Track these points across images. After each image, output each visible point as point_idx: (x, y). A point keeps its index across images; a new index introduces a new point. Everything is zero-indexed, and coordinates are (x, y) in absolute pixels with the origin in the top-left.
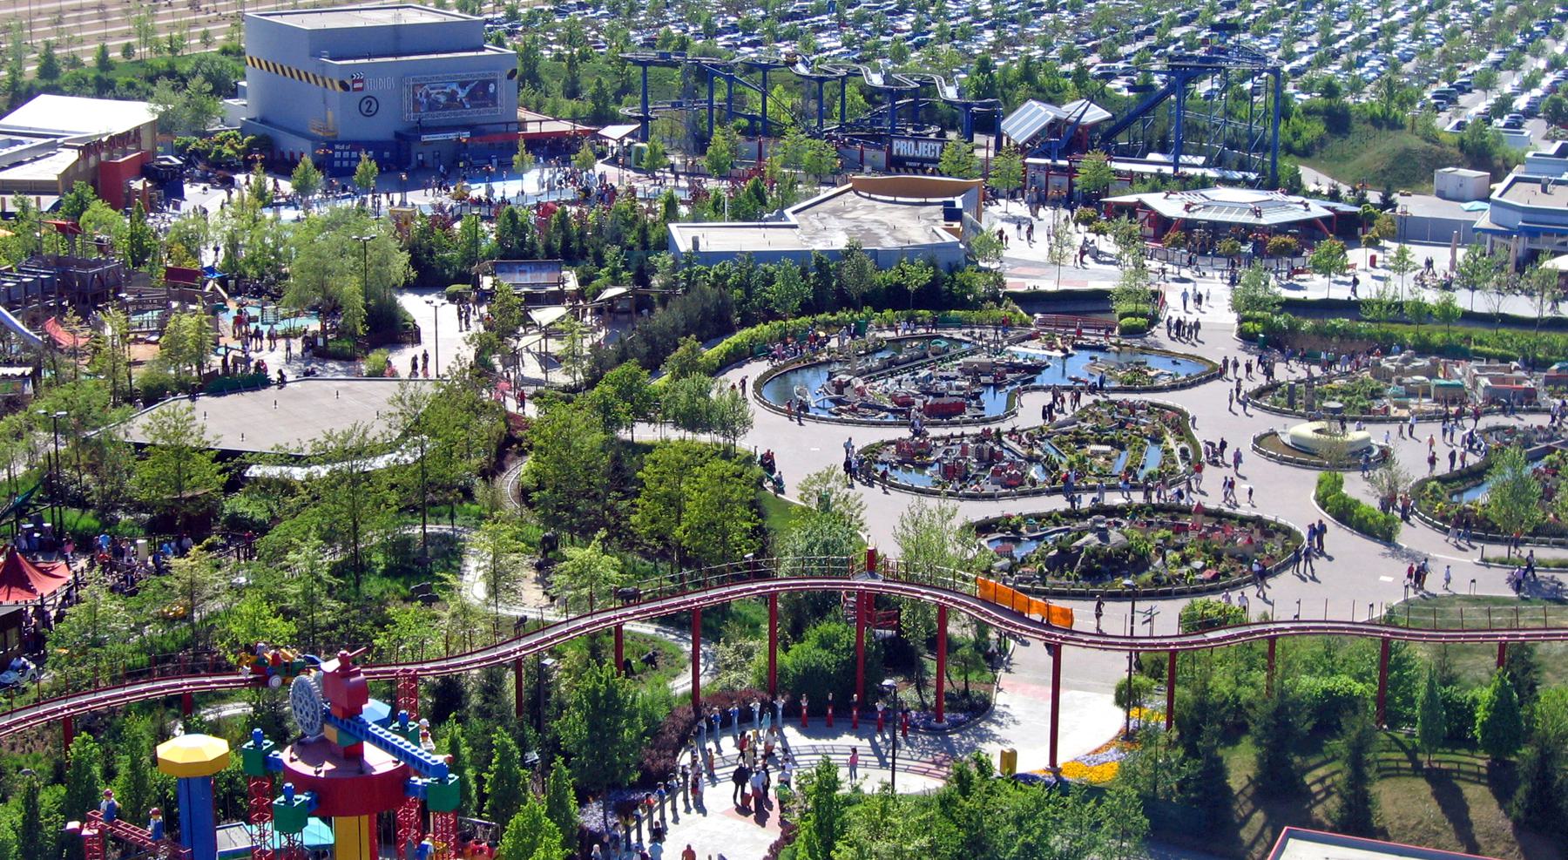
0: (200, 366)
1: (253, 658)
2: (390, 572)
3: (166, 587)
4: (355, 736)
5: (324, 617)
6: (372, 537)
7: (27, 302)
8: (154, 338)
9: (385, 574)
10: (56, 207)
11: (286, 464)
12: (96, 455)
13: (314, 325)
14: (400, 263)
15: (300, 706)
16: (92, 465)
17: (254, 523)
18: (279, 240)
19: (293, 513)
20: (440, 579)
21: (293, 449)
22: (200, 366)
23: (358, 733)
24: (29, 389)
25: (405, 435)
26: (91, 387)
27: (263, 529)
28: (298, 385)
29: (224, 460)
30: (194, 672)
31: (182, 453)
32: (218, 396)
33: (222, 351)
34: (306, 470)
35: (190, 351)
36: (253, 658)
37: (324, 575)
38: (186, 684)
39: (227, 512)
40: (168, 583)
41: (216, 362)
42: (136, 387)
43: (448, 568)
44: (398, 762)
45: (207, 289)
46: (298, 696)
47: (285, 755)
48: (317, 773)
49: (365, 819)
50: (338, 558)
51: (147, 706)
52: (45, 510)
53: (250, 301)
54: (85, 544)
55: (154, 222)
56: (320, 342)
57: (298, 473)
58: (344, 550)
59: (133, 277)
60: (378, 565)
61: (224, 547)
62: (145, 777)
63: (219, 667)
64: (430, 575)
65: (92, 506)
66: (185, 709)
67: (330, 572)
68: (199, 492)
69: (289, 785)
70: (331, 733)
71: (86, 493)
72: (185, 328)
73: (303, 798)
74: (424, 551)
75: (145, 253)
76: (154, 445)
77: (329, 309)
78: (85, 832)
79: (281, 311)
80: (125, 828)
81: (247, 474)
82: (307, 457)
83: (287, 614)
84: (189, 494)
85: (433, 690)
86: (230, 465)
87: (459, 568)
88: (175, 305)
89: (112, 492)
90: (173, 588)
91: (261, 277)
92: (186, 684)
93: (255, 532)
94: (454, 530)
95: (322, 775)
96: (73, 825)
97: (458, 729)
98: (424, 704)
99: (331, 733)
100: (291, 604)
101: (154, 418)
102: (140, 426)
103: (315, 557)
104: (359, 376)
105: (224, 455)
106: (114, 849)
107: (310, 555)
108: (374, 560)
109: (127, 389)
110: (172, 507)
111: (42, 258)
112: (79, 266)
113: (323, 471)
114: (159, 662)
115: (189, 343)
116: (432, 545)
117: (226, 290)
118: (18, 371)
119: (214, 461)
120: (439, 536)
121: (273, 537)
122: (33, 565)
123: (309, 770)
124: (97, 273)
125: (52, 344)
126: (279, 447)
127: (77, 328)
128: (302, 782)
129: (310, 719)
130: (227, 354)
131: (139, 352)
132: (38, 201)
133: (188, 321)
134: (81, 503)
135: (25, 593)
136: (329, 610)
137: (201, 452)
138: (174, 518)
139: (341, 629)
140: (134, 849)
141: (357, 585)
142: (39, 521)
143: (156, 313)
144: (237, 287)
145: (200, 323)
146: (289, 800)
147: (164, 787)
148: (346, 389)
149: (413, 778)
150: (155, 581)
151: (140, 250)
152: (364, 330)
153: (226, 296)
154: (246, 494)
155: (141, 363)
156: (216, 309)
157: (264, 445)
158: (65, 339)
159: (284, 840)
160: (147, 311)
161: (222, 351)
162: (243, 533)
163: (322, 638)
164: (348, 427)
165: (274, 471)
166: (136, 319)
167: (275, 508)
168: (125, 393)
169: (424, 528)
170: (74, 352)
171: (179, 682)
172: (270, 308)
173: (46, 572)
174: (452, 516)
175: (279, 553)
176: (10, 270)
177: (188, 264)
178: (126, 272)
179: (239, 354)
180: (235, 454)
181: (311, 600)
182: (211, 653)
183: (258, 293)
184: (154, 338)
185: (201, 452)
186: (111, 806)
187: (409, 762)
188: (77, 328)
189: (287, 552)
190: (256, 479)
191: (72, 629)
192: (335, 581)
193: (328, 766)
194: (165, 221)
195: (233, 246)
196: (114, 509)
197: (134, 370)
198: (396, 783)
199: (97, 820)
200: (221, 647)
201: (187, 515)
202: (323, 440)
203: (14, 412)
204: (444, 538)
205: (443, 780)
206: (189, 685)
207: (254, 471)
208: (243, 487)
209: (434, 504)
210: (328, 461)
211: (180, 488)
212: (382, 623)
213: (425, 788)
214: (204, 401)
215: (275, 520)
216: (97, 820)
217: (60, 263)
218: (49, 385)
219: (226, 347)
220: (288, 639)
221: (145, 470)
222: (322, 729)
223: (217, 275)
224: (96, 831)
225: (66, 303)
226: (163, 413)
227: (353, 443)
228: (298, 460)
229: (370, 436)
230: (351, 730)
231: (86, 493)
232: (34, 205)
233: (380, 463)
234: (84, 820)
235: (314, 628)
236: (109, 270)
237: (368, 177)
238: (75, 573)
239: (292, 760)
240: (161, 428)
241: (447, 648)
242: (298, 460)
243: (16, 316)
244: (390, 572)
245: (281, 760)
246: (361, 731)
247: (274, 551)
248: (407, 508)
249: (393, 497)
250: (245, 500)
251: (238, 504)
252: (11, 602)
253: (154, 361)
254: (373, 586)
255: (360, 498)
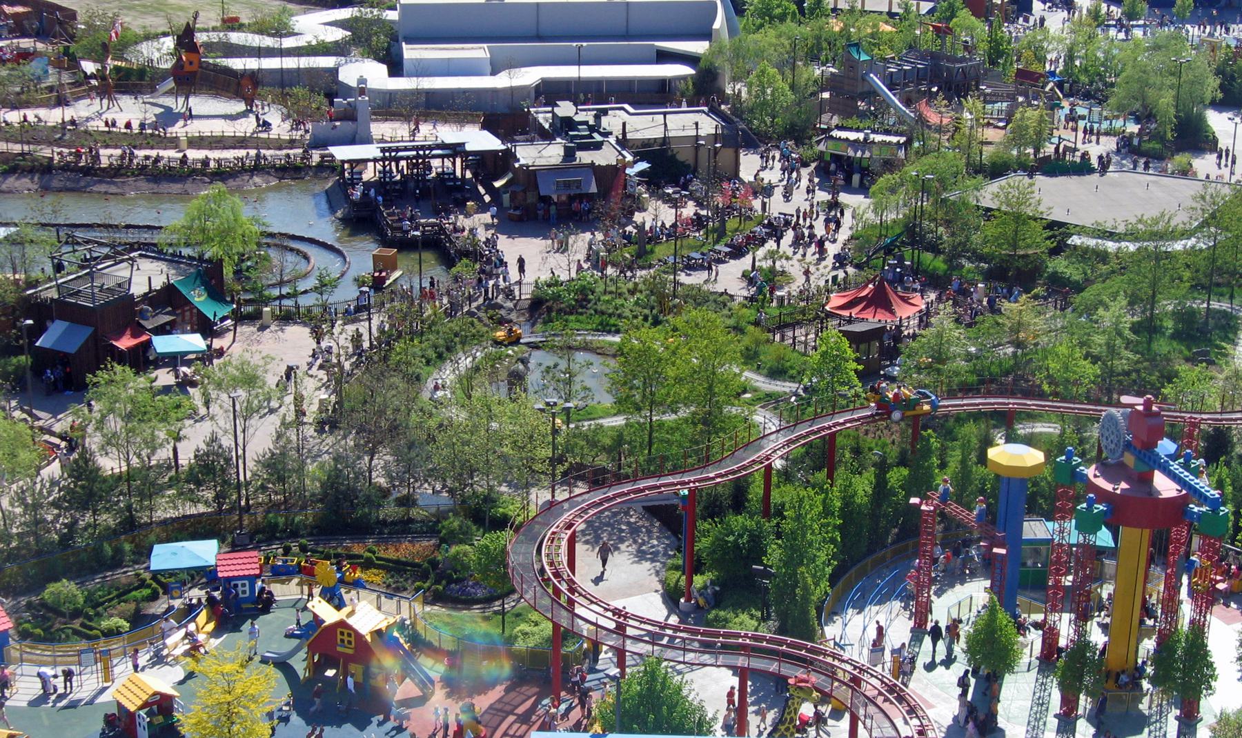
0: (1037, 150)
1: (878, 397)
2: (1176, 336)
3: (998, 324)
4: (1148, 465)
5: (1121, 365)
6: (1168, 305)
7: (906, 85)
8: (1001, 124)
9: (1174, 337)
10: (931, 12)
11: (1099, 238)
12: (953, 215)
13: (1132, 128)
14: (1212, 84)
15: (1107, 434)
16: (947, 221)
17: (1070, 282)
18: (1109, 57)
19: (1106, 277)
20: (1218, 347)
21: (1109, 226)
22: (1037, 150)
23: (1151, 463)
24: (901, 154)
25: (1201, 226)
26: (951, 158)
27: (1079, 288)
28: (1116, 175)
29: (1052, 229)
30: (1013, 394)
31: (1020, 219)
32: (1079, 175)
33: (1055, 140)
34: (1117, 245)
35: (1031, 137)
36: (878, 397)
37: (1127, 332)
38: (1012, 403)
39: (1050, 270)
40: (1000, 321)
41: (1049, 149)
42: (984, 162)
43: (1226, 338)
44: (1181, 491)
45: (1047, 89)
46: (1106, 426)
47: (1090, 471)
48: (1114, 489)
49: (1147, 532)
50: (1136, 319)
51: (977, 416)
52: (907, 252)
53: (1081, 102)
54: (934, 281)
55: (1008, 30)
56: (1136, 142)
57: (1111, 246)
58: (1143, 312)
59: (989, 74)
60: (1167, 329)
61: (1045, 298)
62: (971, 471)
63: (1034, 392)
64: (1210, 342)
65: (943, 253)
66: (1006, 420)
67: (1130, 329)
68: (1030, 252)
69: (1091, 495)
70: (1129, 459)
71: (939, 242)
72: (1029, 119)
73: (1101, 508)
74: (1206, 323)
75: (1000, 54)
76: (999, 210)
77: (1145, 116)
78: (924, 507)
79: (1105, 113)
80: (953, 508)
81: (1069, 242)
82: (1119, 234)
83: (1095, 359)
84: (1022, 253)
85: (1208, 438)
86: (1056, 233)
87: (1233, 341)
88: (1021, 99)
89: (959, 244)
90: (1003, 325)
91: (1091, 83)
92: (1012, 403)
93: (1071, 289)
94: (1232, 308)
95: (1118, 492)
96: (914, 500)
97: (1225, 470)
98: (1197, 445)
99: (1129, 459)
100: (1095, 351)
101: (1001, 188)
102: (990, 194)
103: (1120, 316)
104: (1163, 172)
105: (1053, 225)
106: (939, 523)
107: (1117, 314)
108: (1165, 324)
109: (977, 163)
110: (1008, 261)
111: (919, 51)
112: (948, 61)
113: (1132, 247)
114: (984, 382)
115: (1031, 131)
116: (1213, 318)
117: (1062, 92)
118: (894, 139)
119: (1044, 228)
120: (1219, 312)
121: (1088, 294)
122: (896, 293)
123: (1108, 487)
124: (962, 67)
125: (922, 121)
126: (1098, 224)
127: (943, 110)
128: (1102, 495)
129: (1113, 446)
130: (1060, 143)
131: (990, 134)
132: (918, 5)
133: (1031, 115)
134: (935, 249)
135: (888, 314)
136: (1126, 359)
137: (1035, 219)
138: (1007, 270)
139: (1134, 376)
140: (954, 525)
141: (1150, 342)
142: (901, 260)
143: (1005, 104)
144: (1071, 89)
145: (1042, 116)
146: (1090, 507)
147: (983, 481)
148: (1154, 182)
149: (1191, 506)
150: (989, 318)
151: (996, 52)
152: (1172, 136)
153: (1061, 96)
154: (1067, 258)
155: (990, 143)
156: (1053, 106)
157: (1088, 222)
158: (933, 118)
159: (1081, 538)
160: (997, 102)
161: (1055, 140)
162: (1061, 289)
163: (1118, 381)
164: (1155, 213)
165: (1092, 242)
166: (989, 107)
167: (1089, 272)
168: (976, 166)
169: (1208, 304)
170: (940, 129)
171: (1006, 401)
172: (1096, 109)
173: (905, 300)
174: (1232, 297)
175: (1090, 310)
176: (893, 58)
177: (1035, 67)
178: (984, 69)
179: (1070, 145)
180: (1061, 225)
181: (1111, 348)
182: (1027, 381)
183: (1087, 96)
184: (1001, 124)
185: (1035, 219)
186: (946, 490)
187: (1191, 492)
188: (943, 110)
189: (1097, 309)
190: (1075, 247)
191: (922, 347)
192: (1132, 337)
193: (1124, 485)
194: (1015, 31)
195: (1070, 58)
196: (960, 256)
197: (985, 148)
198: (1177, 508)
199: (933, 499)
200: (1039, 377)
201: (1018, 269)
202: (1133, 220)
203: (892, 172)
204: (1224, 314)
205: (1215, 510)
206: (1014, 404)
207: (1075, 240)
208: (1064, 251)
209: (1218, 285)
210: (1136, 239)
211: (1015, 246)
212: (1170, 377)
213: (1201, 515)
214: (1040, 179)
215: (1088, 282)
216: (933, 499)
217: (934, 57)
218: (917, 153)
219: (1060, 138)
220: (1092, 378)
221: (991, 229)
222: (1122, 455)
223: (1057, 79)
224: (932, 508)
225: (935, 89)
226: (1009, 185)
227: (1161, 226)
228: (1111, 236)
229: (1173, 223)
230: (1146, 460)
231: (939, 242)
232: (914, 8)
233: (1178, 246)
234: (924, 498)
235: (1111, 372)
236: (971, 66)
237: (1184, 10)
238: (928, 303)
239: (1095, 476)
240: (1007, 197)
241: (1222, 404)
242: (1111, 236)
243: (894, 95)
244: (1176, 336)
245: (1086, 475)
246: (1155, 462)
247: (1086, 307)
248: (1196, 285)
249: (1187, 274)
250: (1065, 263)
251: (1060, 265)
252: (876, 320)
253: (1001, 143)
254: (1162, 346)
255: (1160, 272)
